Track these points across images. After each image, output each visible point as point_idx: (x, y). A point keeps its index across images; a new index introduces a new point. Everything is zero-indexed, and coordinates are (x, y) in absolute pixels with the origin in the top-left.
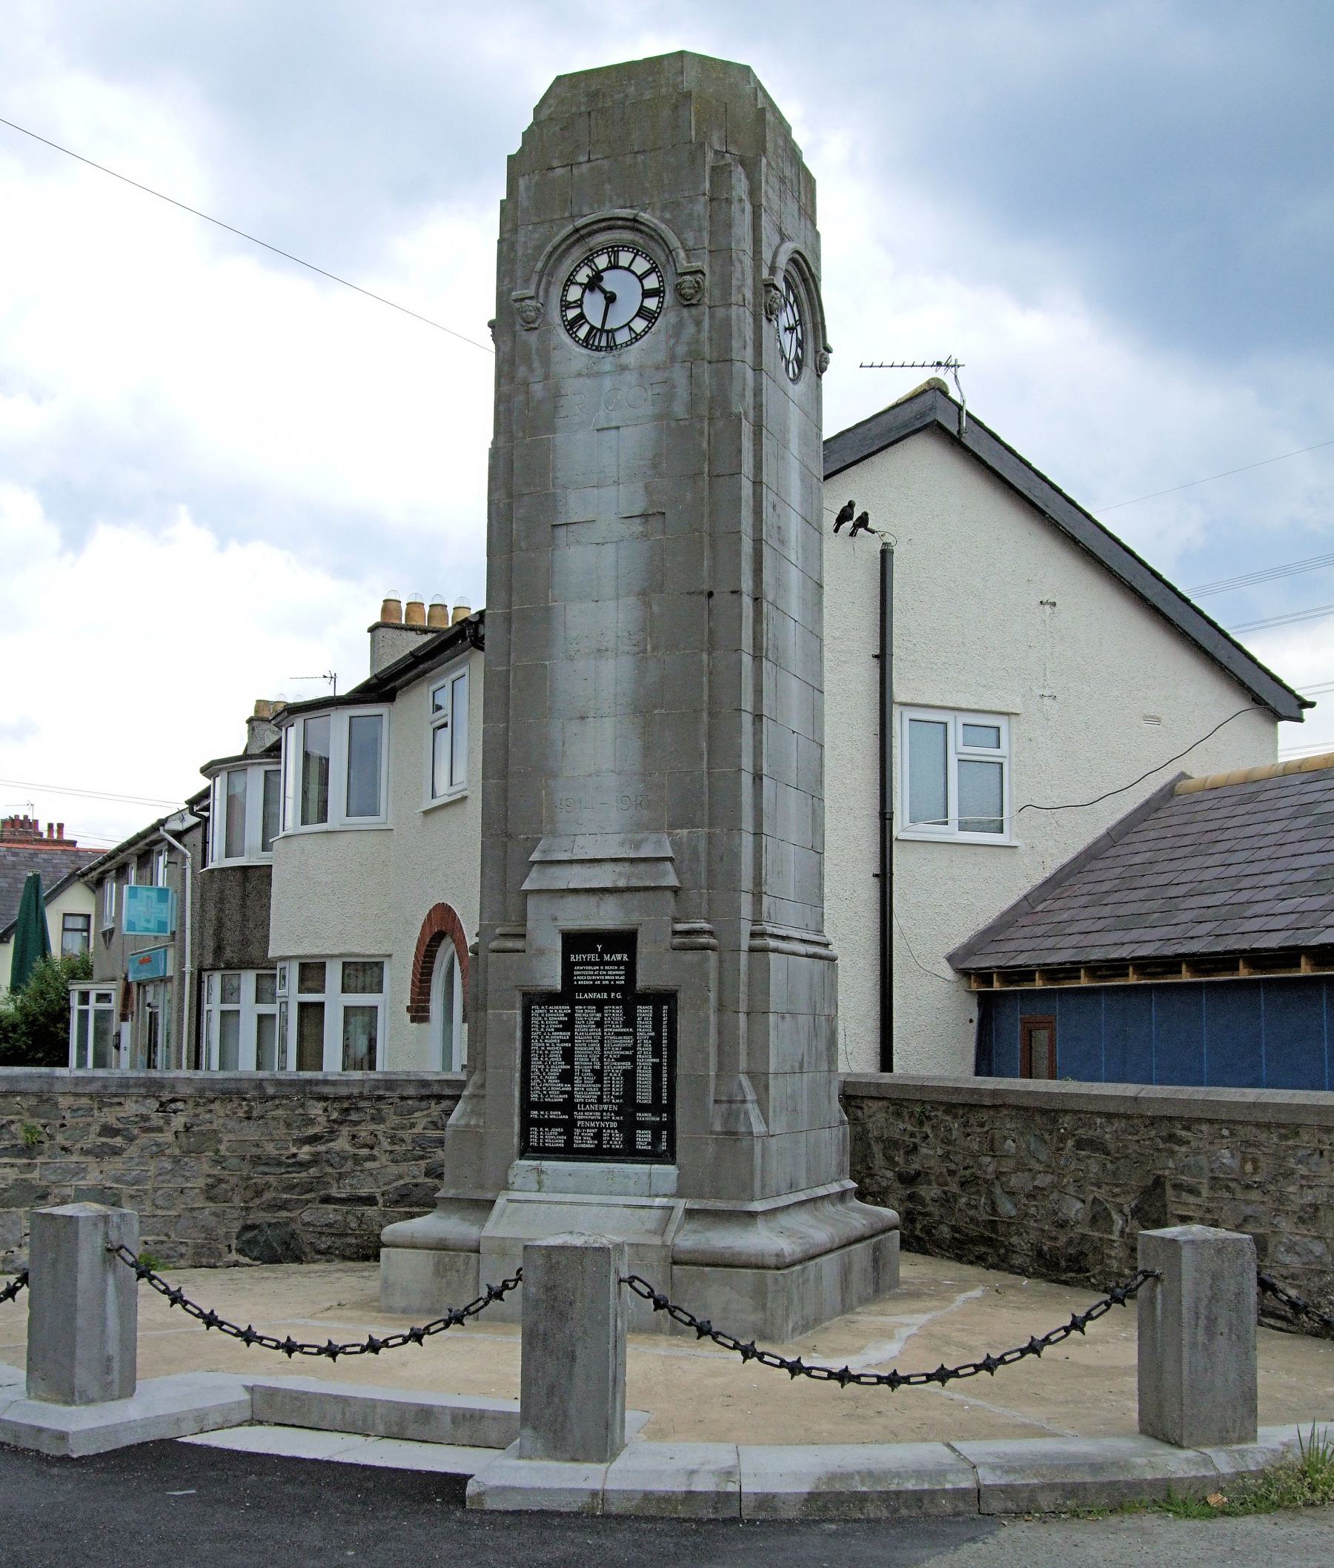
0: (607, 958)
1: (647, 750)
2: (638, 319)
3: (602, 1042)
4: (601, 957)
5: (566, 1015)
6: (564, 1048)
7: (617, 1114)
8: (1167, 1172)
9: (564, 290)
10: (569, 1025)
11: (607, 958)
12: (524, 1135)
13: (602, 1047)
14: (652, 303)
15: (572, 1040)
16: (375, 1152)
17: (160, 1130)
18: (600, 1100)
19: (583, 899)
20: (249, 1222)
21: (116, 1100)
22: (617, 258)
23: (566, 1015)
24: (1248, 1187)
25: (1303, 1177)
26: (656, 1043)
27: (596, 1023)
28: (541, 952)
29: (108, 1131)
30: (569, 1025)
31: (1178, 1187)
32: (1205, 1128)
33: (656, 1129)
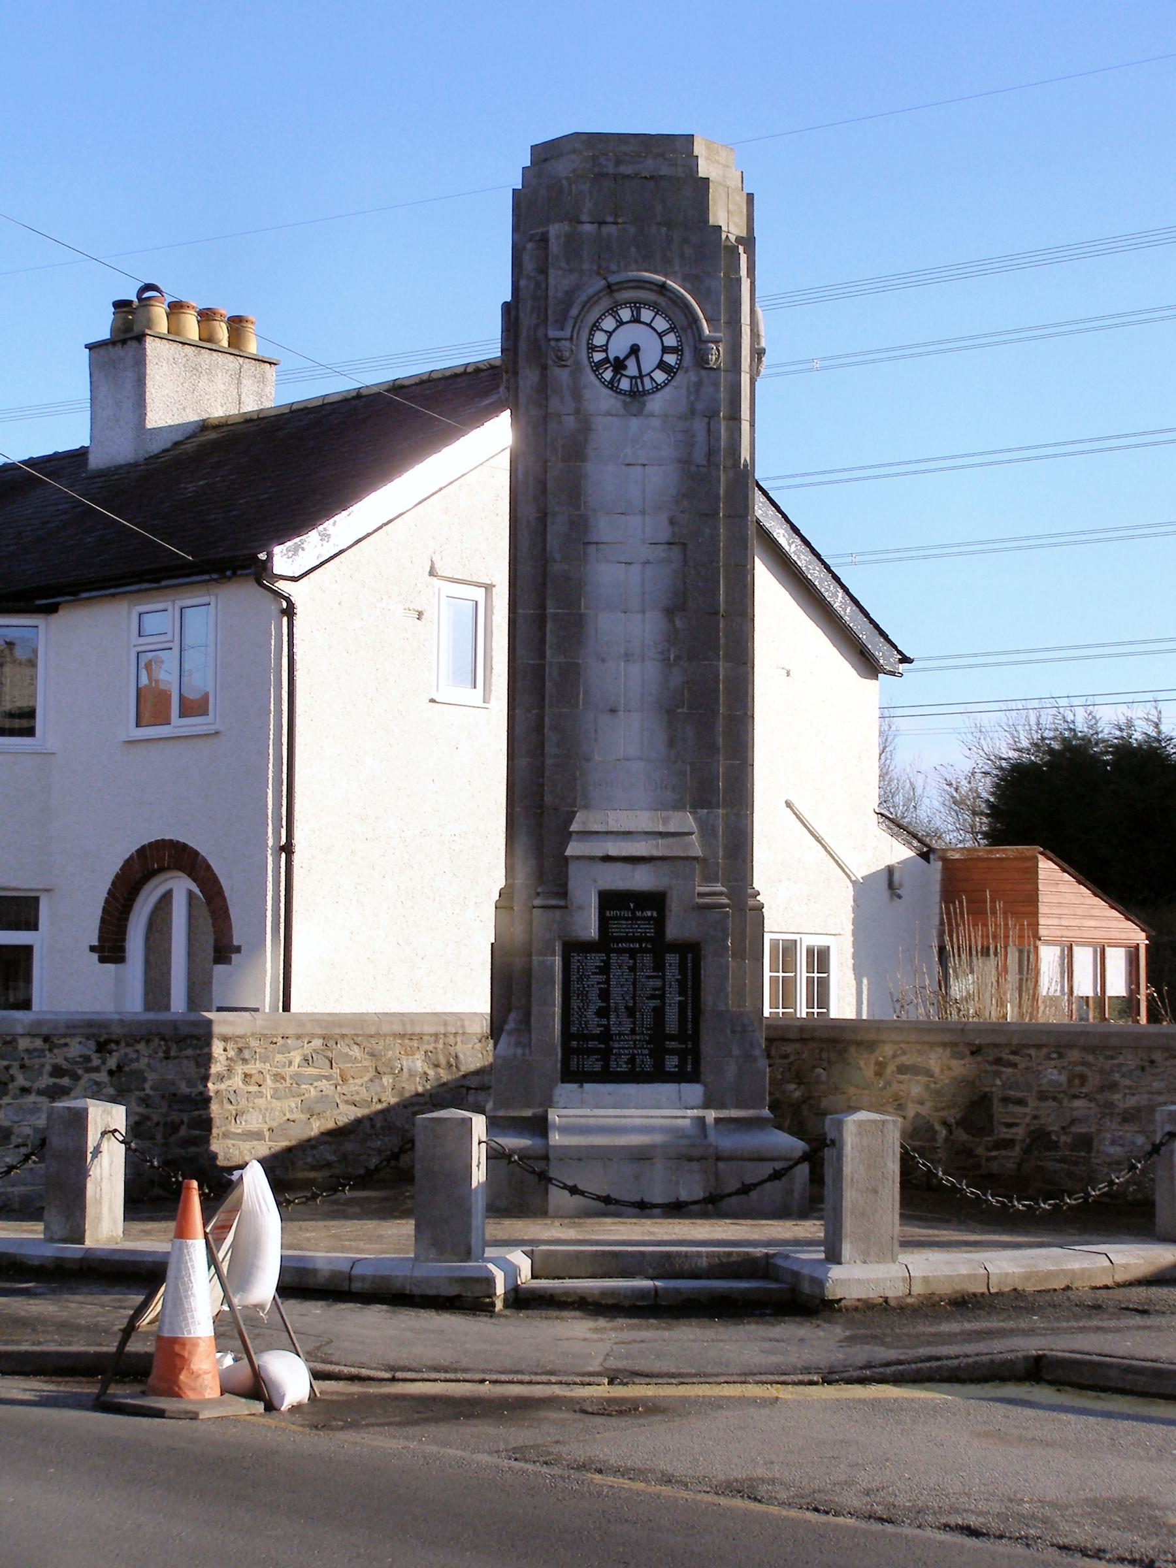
0: (638, 914)
1: (671, 743)
2: (657, 371)
3: (634, 984)
4: (633, 913)
5: (602, 961)
6: (600, 989)
7: (648, 1042)
8: (994, 1089)
9: (591, 334)
10: (605, 969)
11: (638, 914)
12: (565, 1061)
13: (635, 987)
14: (671, 359)
15: (607, 981)
16: (262, 1089)
17: (97, 1070)
18: (633, 1032)
19: (619, 866)
20: (169, 1157)
21: (63, 1041)
22: (639, 313)
23: (602, 961)
24: (1075, 1097)
25: (1126, 1087)
26: (682, 984)
27: (629, 968)
28: (581, 908)
29: (57, 1071)
30: (605, 969)
31: (1006, 1100)
32: (1032, 1052)
33: (682, 1055)
